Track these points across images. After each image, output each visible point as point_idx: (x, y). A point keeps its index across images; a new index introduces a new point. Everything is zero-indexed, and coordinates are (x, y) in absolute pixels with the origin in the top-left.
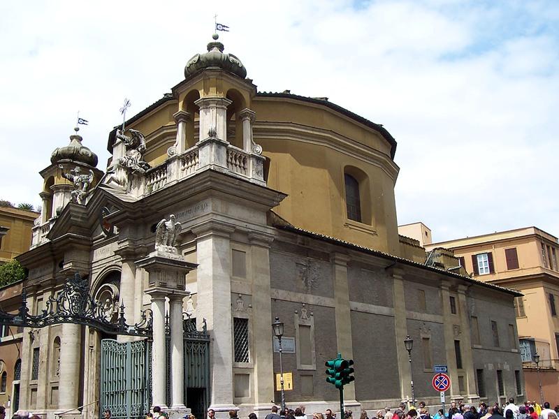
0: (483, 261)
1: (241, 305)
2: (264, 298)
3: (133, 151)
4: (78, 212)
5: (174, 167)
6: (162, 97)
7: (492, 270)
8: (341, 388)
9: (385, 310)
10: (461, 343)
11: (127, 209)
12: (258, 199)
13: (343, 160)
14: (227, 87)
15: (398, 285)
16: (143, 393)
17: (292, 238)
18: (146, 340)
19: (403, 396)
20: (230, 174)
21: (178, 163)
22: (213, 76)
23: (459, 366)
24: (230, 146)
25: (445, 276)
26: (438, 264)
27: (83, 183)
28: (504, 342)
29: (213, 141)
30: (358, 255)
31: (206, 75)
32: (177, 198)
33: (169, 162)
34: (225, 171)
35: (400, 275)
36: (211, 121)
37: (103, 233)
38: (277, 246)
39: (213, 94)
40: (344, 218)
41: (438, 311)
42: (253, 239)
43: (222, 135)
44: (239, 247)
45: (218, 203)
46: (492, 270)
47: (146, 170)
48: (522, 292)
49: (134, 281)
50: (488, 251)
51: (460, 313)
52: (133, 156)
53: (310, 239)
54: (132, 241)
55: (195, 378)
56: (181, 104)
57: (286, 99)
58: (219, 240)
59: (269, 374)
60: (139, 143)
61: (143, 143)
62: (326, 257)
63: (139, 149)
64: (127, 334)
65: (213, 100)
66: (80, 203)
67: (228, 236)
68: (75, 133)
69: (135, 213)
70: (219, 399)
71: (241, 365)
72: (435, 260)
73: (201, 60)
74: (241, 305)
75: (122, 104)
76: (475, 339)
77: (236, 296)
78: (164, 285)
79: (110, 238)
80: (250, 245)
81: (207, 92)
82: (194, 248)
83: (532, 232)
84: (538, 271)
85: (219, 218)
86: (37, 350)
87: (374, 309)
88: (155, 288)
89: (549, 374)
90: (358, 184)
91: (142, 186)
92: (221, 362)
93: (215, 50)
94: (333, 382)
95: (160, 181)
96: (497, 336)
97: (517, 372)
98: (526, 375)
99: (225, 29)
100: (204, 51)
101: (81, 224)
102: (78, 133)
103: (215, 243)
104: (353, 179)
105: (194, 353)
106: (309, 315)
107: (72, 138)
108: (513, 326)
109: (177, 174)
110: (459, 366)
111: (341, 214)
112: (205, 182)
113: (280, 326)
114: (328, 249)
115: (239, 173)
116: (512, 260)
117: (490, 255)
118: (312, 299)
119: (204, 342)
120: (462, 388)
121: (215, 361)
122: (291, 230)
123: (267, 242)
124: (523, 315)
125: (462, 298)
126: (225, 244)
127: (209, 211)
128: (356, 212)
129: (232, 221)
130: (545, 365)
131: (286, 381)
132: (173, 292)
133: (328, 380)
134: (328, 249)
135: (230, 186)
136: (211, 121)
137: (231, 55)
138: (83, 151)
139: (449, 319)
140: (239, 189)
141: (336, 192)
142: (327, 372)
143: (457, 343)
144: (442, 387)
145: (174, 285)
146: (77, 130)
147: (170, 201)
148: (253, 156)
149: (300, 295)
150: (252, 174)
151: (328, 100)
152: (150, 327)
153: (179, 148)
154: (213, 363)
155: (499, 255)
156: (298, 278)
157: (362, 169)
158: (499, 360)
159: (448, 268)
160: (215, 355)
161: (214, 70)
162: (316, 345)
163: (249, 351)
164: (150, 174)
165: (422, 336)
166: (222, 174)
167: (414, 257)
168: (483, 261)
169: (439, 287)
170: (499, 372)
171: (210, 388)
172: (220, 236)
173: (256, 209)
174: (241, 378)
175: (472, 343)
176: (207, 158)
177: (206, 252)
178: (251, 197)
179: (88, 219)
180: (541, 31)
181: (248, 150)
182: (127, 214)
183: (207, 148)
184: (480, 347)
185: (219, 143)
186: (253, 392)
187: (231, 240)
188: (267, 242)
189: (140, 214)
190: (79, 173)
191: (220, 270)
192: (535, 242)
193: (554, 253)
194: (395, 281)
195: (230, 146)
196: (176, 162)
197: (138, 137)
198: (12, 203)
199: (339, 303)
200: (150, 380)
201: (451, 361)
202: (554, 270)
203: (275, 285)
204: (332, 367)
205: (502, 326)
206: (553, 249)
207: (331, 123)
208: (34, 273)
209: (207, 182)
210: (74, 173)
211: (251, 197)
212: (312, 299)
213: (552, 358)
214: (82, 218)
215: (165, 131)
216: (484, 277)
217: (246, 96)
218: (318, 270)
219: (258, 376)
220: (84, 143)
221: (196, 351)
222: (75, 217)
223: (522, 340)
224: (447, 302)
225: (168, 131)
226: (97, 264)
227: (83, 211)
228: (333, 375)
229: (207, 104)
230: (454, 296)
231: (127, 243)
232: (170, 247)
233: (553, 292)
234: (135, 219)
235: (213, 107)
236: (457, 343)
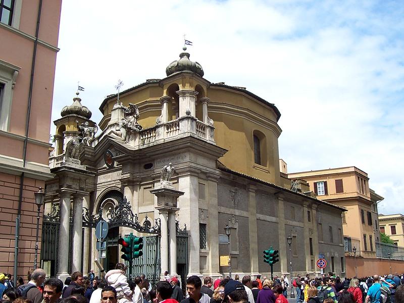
0: (321, 187)
1: (203, 216)
3: (131, 117)
4: (89, 152)
5: (162, 131)
6: (145, 81)
7: (326, 193)
8: (271, 265)
9: (274, 219)
10: (313, 240)
11: (130, 154)
12: (213, 153)
13: (252, 126)
14: (195, 84)
15: (281, 204)
16: (155, 266)
17: (229, 176)
18: (157, 236)
19: (282, 271)
20: (198, 138)
21: (164, 128)
22: (188, 77)
23: (312, 254)
24: (198, 120)
25: (305, 198)
26: (299, 190)
27: (91, 133)
28: (336, 239)
29: (188, 118)
30: (261, 186)
31: (183, 75)
32: (166, 150)
33: (157, 127)
34: (196, 136)
35: (282, 198)
36: (187, 105)
37: (105, 166)
38: (221, 181)
39: (188, 88)
40: (253, 163)
41: (301, 220)
42: (209, 177)
43: (193, 114)
44: (202, 182)
45: (192, 155)
46: (326, 193)
47: (140, 130)
48: (347, 208)
49: (133, 198)
50: (325, 181)
51: (313, 222)
52: (132, 120)
53: (237, 176)
54: (132, 174)
55: (46, 252)
56: (165, 91)
57: (221, 88)
58: (193, 177)
59: (217, 256)
60: (135, 111)
61: (138, 112)
62: (244, 187)
63: (135, 116)
64: (150, 233)
65: (188, 92)
66: (89, 145)
67: (197, 175)
68: (76, 96)
69: (135, 157)
70: (193, 270)
71: (203, 250)
72: (296, 187)
73: (179, 65)
74: (203, 216)
75: (117, 84)
76: (320, 237)
77: (201, 210)
78: (167, 205)
79: (111, 169)
80: (207, 180)
81: (184, 86)
82: (176, 181)
83: (353, 170)
84: (355, 195)
85: (193, 165)
87: (268, 218)
88: (162, 206)
89: (359, 260)
90: (259, 140)
91: (137, 140)
92: (194, 249)
93: (185, 58)
94: (268, 262)
95: (150, 138)
96: (332, 236)
97: (342, 258)
98: (347, 260)
99: (190, 43)
100: (178, 59)
101: (90, 159)
102: (78, 97)
103: (191, 180)
104: (257, 138)
105: (52, 233)
107: (74, 100)
108: (341, 230)
109: (163, 136)
110: (312, 254)
111: (251, 160)
112: (186, 143)
113: (224, 229)
114: (246, 182)
115: (202, 137)
116: (339, 187)
117: (325, 183)
118: (237, 212)
119: (185, 238)
120: (313, 268)
121: (191, 249)
122: (229, 171)
123: (216, 178)
124: (345, 222)
125: (314, 212)
126: (196, 180)
127: (186, 161)
128: (258, 160)
129: (199, 166)
130: (357, 254)
131: (225, 260)
132: (76, 192)
133: (265, 261)
134: (246, 182)
135: (200, 146)
136: (187, 105)
137: (196, 63)
138: (84, 109)
139: (308, 225)
140: (204, 148)
141: (249, 146)
142: (265, 257)
143: (311, 239)
144: (321, 266)
145: (172, 204)
146: (78, 94)
147: (161, 151)
148: (209, 126)
149: (231, 210)
150: (208, 138)
151: (246, 89)
152: (160, 229)
153: (164, 118)
154: (190, 250)
155: (331, 183)
156: (231, 200)
157: (260, 130)
158: (332, 250)
159: (303, 192)
160: (191, 245)
161: (190, 73)
162: (239, 239)
163: (206, 243)
164: (142, 133)
165: (293, 235)
166: (194, 138)
167: (285, 185)
168: (321, 187)
169: (302, 205)
170: (332, 258)
171: (188, 264)
172: (193, 175)
173: (211, 159)
174: (203, 257)
175: (319, 240)
176: (185, 129)
177: (185, 184)
178: (210, 152)
179: (95, 156)
180: (344, 24)
181: (206, 123)
182: (130, 157)
183: (185, 122)
184: (323, 242)
185: (192, 119)
186: (208, 267)
187: (199, 178)
188: (216, 178)
189: (138, 157)
190: (88, 126)
191: (193, 196)
192: (354, 176)
193: (365, 184)
194: (280, 201)
195: (198, 120)
196: (163, 128)
197: (134, 108)
199: (251, 214)
200: (160, 260)
201: (307, 251)
202: (365, 194)
203: (220, 204)
204: (267, 254)
205: (335, 229)
206: (365, 181)
207: (246, 103)
208: (51, 187)
209: (188, 143)
210: (84, 126)
211: (210, 152)
212: (237, 212)
213: (361, 250)
214: (91, 155)
215: (148, 104)
216: (321, 197)
217: (205, 88)
218: (241, 195)
219: (212, 257)
220: (83, 103)
221: (48, 231)
222: (87, 154)
223: (346, 238)
224: (306, 214)
225: (150, 104)
226: (100, 185)
227: (92, 151)
228: (267, 258)
229: (184, 94)
230: (309, 211)
231: (129, 175)
232: (169, 182)
233: (363, 209)
234: (134, 160)
235: (188, 96)
236: (311, 239)
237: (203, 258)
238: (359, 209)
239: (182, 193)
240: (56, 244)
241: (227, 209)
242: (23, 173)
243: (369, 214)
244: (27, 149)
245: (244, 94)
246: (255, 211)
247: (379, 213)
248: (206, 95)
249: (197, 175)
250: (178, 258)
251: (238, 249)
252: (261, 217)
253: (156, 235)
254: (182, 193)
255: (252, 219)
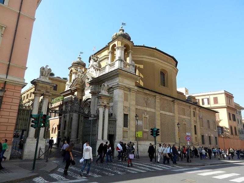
0: (206, 101)
2: (133, 108)
9: (171, 114)
46: (209, 103)
67: (123, 89)
68: (79, 57)
71: (59, 131)
76: (202, 125)
86: (65, 121)
87: (168, 113)
106: (147, 114)
118: (148, 109)
119: (114, 121)
129: (124, 85)
148: (132, 65)
160: (118, 125)
168: (206, 101)
175: (200, 127)
176: (117, 65)
184: (203, 128)
198: (61, 77)
203: (137, 104)
205: (211, 122)
206: (231, 98)
212: (148, 109)
216: (206, 105)
221: (23, 114)
233: (230, 112)
236: (195, 126)
237: (125, 132)
238: (227, 112)
239: (27, 84)
240: (28, 121)
241: (142, 107)
242: (6, 81)
243: (234, 116)
244: (9, 70)
245: (155, 50)
246: (159, 109)
247: (225, 109)
248: (131, 49)
249: (123, 89)
250: (109, 131)
251: (148, 128)
252: (163, 112)
253: (95, 118)
254: (27, 84)
255: (158, 113)
